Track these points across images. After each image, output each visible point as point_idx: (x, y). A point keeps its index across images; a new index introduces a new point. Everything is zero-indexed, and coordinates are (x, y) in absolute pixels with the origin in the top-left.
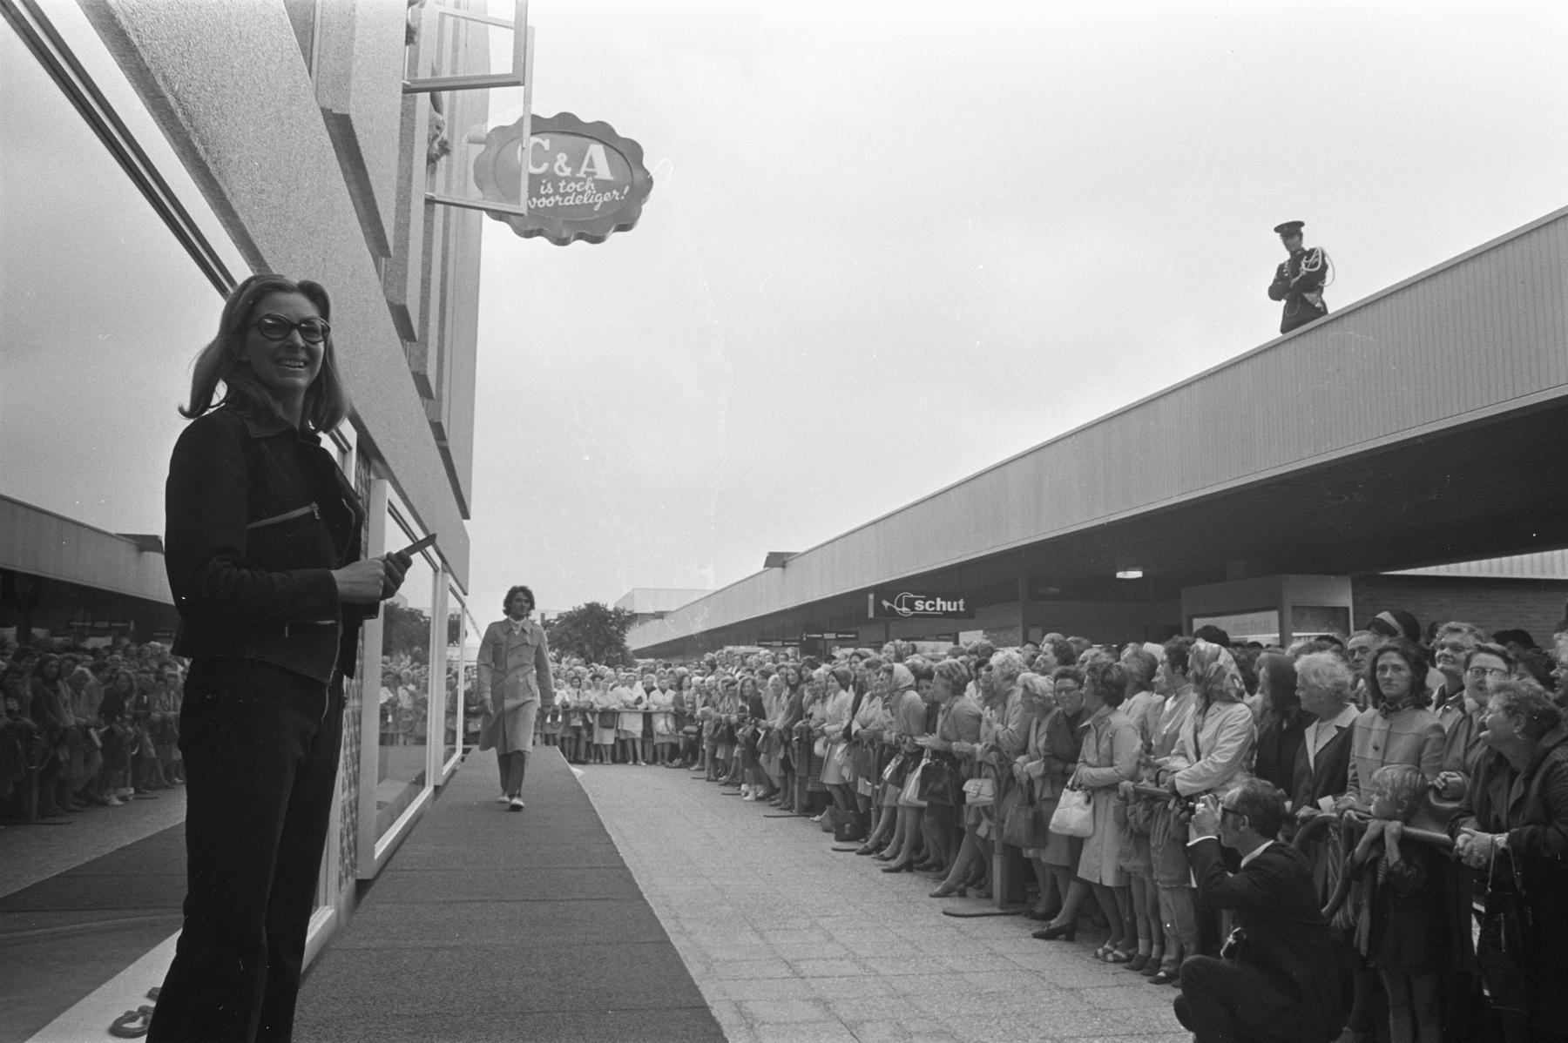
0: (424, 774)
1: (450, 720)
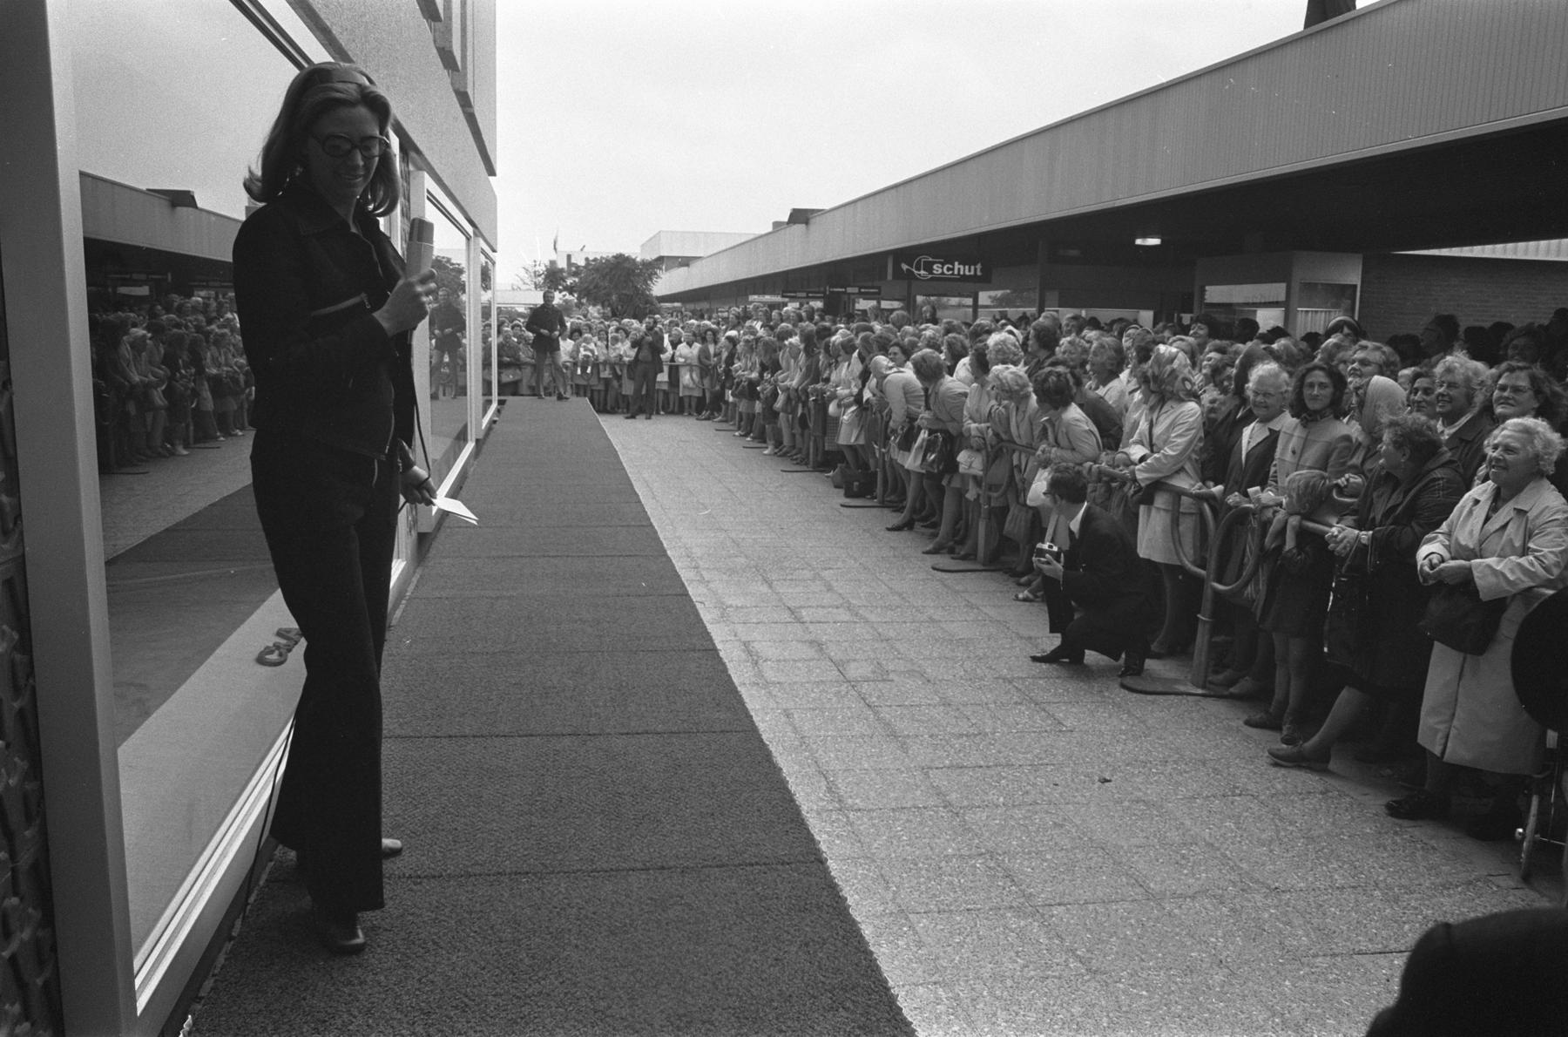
0: (465, 427)
1: (486, 371)
